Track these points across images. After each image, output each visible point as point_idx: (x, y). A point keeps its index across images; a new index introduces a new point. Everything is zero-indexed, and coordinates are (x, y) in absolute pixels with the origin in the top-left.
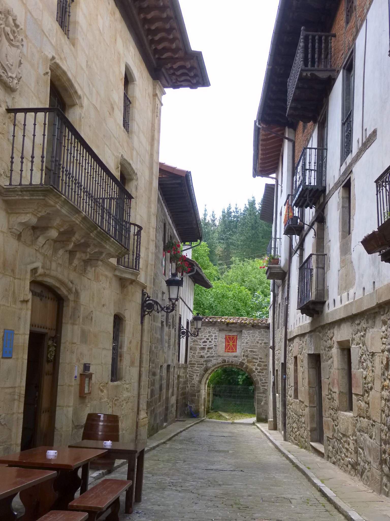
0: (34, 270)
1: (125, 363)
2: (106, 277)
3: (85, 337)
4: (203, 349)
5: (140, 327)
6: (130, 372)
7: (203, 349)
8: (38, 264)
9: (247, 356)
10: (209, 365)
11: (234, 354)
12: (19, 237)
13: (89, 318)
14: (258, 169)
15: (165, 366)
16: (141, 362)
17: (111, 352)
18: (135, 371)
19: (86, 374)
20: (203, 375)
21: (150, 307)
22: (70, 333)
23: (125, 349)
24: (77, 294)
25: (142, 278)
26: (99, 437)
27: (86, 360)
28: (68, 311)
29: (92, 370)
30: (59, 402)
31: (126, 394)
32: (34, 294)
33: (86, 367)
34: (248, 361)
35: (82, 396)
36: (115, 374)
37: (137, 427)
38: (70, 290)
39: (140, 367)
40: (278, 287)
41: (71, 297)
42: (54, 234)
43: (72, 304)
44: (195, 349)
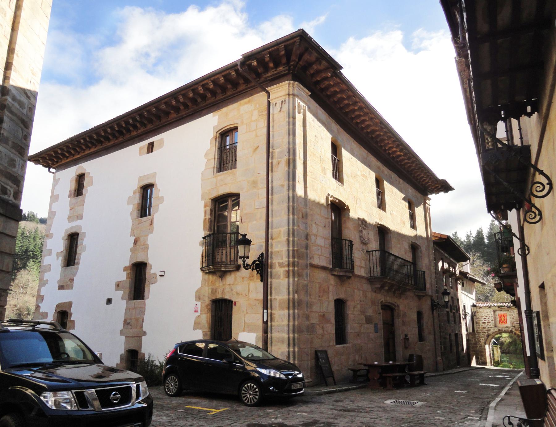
0: (382, 301)
1: (426, 333)
2: (411, 296)
3: (404, 323)
4: (485, 323)
5: (431, 316)
6: (429, 338)
7: (485, 323)
8: (383, 299)
9: (514, 327)
10: (490, 332)
11: (506, 325)
12: (375, 292)
13: (405, 315)
14: (132, 296)
15: (453, 334)
16: (434, 332)
17: (417, 329)
18: (431, 337)
19: (406, 338)
20: (487, 339)
21: (435, 306)
22: (398, 322)
23: (425, 327)
24: (398, 306)
25: (429, 292)
26: (407, 366)
27: (405, 333)
28: (396, 313)
29: (409, 336)
30: (396, 349)
31: (428, 348)
32: (382, 309)
33: (406, 335)
34: (515, 330)
35: (406, 348)
36: (421, 338)
37: (437, 364)
38: (395, 306)
39: (435, 335)
40: (32, 326)
41: (396, 308)
42: (387, 288)
43: (397, 311)
44: (479, 323)
